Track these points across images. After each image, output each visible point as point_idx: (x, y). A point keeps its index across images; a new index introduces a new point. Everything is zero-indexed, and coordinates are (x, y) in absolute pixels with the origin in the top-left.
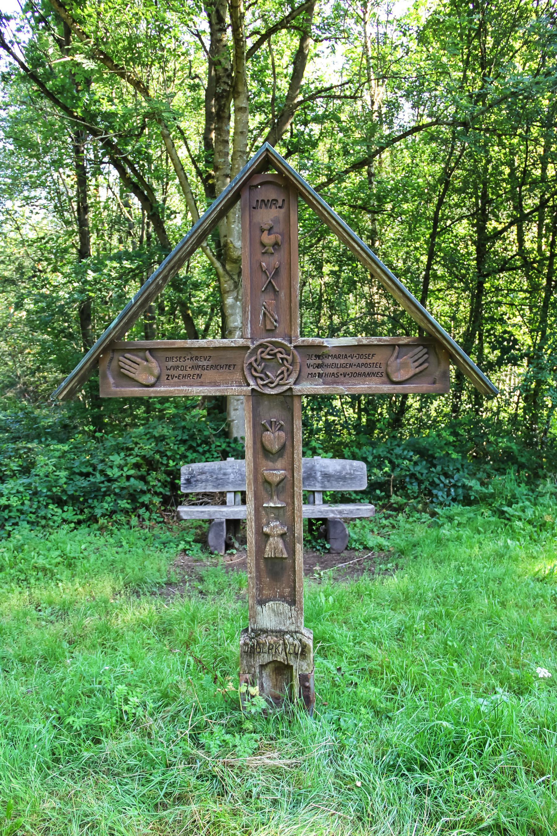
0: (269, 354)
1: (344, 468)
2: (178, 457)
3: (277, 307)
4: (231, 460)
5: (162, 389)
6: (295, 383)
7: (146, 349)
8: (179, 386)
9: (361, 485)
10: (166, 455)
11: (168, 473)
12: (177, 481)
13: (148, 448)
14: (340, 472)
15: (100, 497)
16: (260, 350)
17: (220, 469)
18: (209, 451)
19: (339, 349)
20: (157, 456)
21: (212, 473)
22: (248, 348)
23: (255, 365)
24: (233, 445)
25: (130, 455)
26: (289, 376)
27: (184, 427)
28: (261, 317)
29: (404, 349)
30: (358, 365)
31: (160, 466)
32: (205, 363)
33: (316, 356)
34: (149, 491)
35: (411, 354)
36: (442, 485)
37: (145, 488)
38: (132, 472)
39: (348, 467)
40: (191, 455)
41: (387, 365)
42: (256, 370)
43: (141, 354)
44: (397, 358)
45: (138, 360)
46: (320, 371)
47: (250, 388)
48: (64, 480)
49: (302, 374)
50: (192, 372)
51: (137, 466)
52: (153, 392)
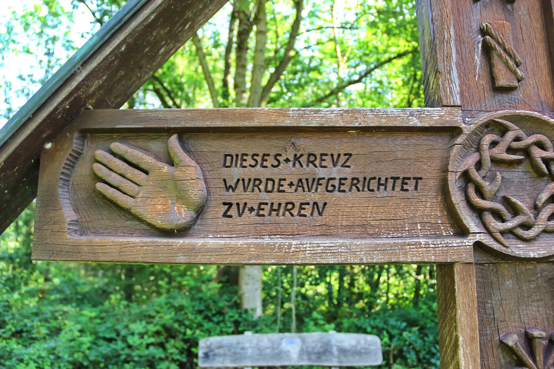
0: (510, 150)
1: (358, 342)
2: (195, 325)
4: (248, 334)
5: (211, 242)
7: (170, 131)
8: (260, 235)
9: (376, 360)
10: (184, 325)
11: (185, 341)
12: (193, 350)
13: (168, 317)
14: (355, 347)
15: (120, 363)
17: (238, 343)
18: (223, 321)
20: (176, 325)
21: (230, 347)
23: (476, 176)
24: (244, 316)
25: (151, 323)
27: (201, 299)
31: (178, 334)
32: (336, 172)
34: (167, 358)
37: (163, 356)
38: (152, 340)
39: (362, 342)
40: (207, 325)
43: (156, 145)
45: (147, 160)
47: (469, 241)
48: (89, 345)
50: (297, 197)
51: (158, 333)
52: (181, 249)
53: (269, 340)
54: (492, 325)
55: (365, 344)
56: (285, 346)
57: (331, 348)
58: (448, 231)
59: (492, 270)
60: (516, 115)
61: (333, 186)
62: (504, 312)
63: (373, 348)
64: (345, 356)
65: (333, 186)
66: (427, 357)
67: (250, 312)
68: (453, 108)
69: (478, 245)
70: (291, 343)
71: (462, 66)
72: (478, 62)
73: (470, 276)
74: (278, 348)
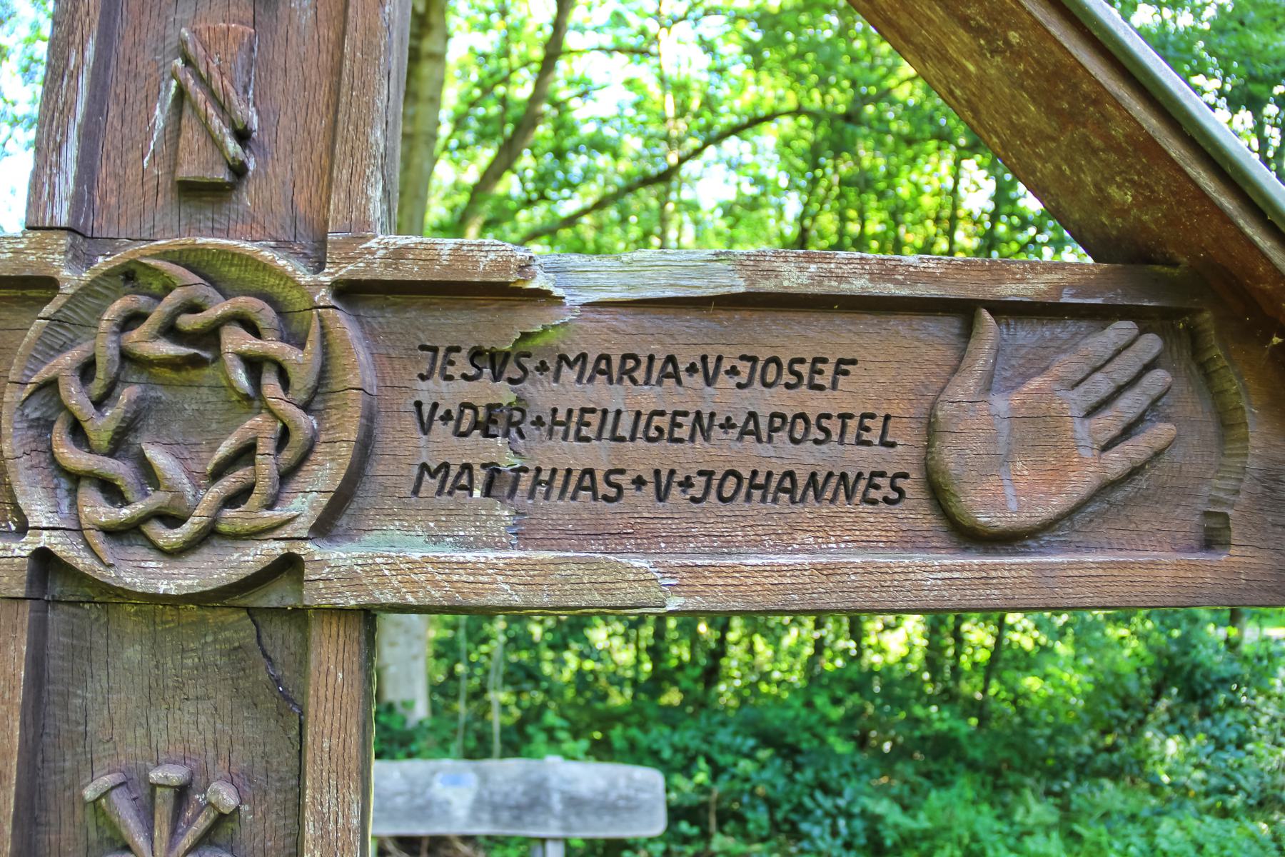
0: (170, 331)
1: (613, 784)
3: (257, 65)
6: (324, 528)
9: (651, 825)
14: (605, 793)
16: (118, 307)
19: (625, 321)
22: (50, 284)
26: (287, 476)
28: (160, 116)
29: (1026, 335)
30: (751, 427)
33: (476, 354)
35: (1068, 364)
36: (819, 813)
39: (622, 782)
41: (931, 428)
42: (77, 431)
44: (988, 385)
46: (499, 450)
49: (379, 468)
53: (404, 775)
54: (79, 750)
55: (628, 787)
56: (440, 790)
57: (548, 796)
58: (6, 521)
59: (97, 619)
60: (196, 250)
61: (658, 429)
62: (111, 720)
63: (645, 796)
64: (579, 814)
65: (658, 429)
66: (794, 817)
67: (399, 709)
68: (49, 233)
69: (43, 558)
70: (455, 781)
71: (117, 133)
72: (160, 124)
73: (14, 629)
74: (423, 793)
